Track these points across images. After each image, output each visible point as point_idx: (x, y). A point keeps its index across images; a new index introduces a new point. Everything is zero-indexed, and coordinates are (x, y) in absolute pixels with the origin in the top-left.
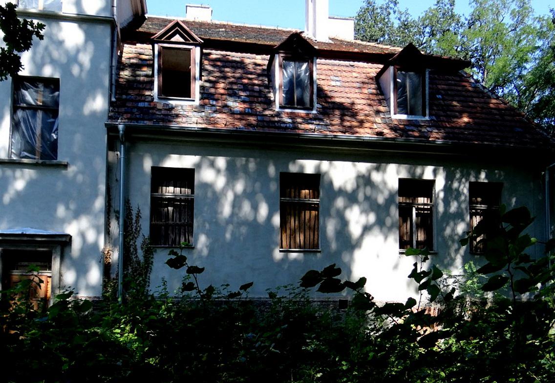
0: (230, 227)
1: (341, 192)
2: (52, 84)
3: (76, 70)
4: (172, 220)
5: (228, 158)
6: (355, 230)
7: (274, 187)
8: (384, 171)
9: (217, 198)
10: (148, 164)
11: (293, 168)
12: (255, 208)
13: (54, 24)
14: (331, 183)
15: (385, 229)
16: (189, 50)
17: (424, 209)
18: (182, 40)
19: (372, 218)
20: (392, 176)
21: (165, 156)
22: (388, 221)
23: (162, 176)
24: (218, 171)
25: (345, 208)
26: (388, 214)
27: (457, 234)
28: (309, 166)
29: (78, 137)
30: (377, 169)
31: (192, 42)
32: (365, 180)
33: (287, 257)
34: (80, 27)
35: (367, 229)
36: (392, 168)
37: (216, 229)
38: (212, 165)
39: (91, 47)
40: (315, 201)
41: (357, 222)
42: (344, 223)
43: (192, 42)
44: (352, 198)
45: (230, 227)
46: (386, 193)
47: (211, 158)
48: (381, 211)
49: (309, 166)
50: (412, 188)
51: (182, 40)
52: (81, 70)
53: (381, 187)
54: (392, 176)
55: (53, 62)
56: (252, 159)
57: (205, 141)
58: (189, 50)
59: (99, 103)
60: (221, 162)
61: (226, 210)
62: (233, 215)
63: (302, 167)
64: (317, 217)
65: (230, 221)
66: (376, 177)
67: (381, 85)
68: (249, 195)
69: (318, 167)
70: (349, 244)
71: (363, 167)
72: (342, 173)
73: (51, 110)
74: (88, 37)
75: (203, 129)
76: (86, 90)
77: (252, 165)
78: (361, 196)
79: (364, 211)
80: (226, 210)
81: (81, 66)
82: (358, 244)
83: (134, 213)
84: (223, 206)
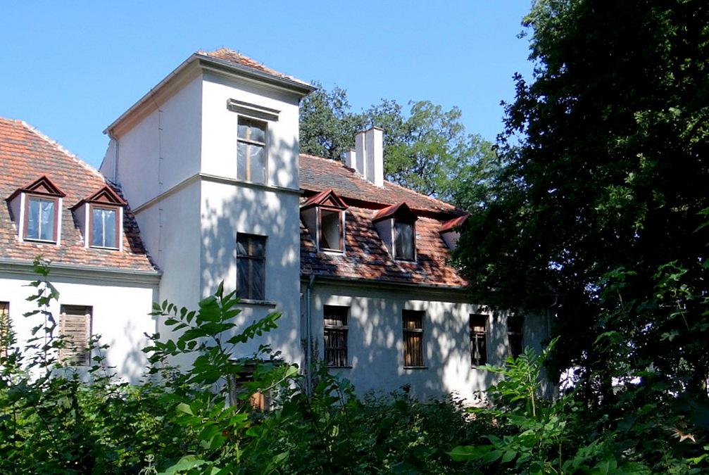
0: (372, 352)
1: (436, 324)
2: (261, 240)
3: (275, 229)
4: (339, 342)
5: (369, 299)
6: (445, 352)
7: (397, 320)
8: (460, 309)
9: (362, 329)
10: (319, 304)
11: (407, 307)
12: (386, 337)
13: (260, 192)
14: (430, 318)
15: (461, 351)
16: (338, 212)
17: (481, 335)
18: (332, 205)
19: (454, 343)
20: (465, 312)
21: (328, 297)
22: (463, 346)
23: (330, 312)
24: (362, 309)
25: (439, 335)
26: (462, 340)
27: (501, 354)
28: (417, 305)
29: (278, 283)
30: (456, 307)
31: (116, 203)
32: (448, 316)
33: (406, 372)
34: (277, 195)
35: (451, 351)
36: (464, 306)
37: (364, 352)
38: (359, 304)
39: (284, 213)
40: (420, 330)
41: (445, 346)
42: (437, 347)
43: (116, 203)
44: (442, 328)
45: (372, 352)
46: (461, 325)
47: (359, 298)
48: (458, 337)
49: (417, 305)
50: (476, 320)
51: (332, 205)
52: (279, 230)
53: (458, 320)
54: (465, 312)
55: (261, 223)
56: (383, 300)
57: (355, 287)
58: (338, 212)
59: (292, 256)
60: (364, 301)
61: (369, 339)
62: (373, 341)
63: (412, 306)
64: (420, 343)
65: (371, 347)
66: (455, 313)
67: (141, 235)
68: (382, 327)
69: (422, 306)
70: (441, 364)
71: (448, 305)
72: (436, 310)
73: (259, 259)
74: (283, 204)
75: (360, 279)
76: (285, 244)
77: (383, 304)
78: (447, 327)
79: (449, 339)
80: (369, 339)
81: (279, 226)
82: (446, 363)
83: (314, 341)
84: (366, 335)
